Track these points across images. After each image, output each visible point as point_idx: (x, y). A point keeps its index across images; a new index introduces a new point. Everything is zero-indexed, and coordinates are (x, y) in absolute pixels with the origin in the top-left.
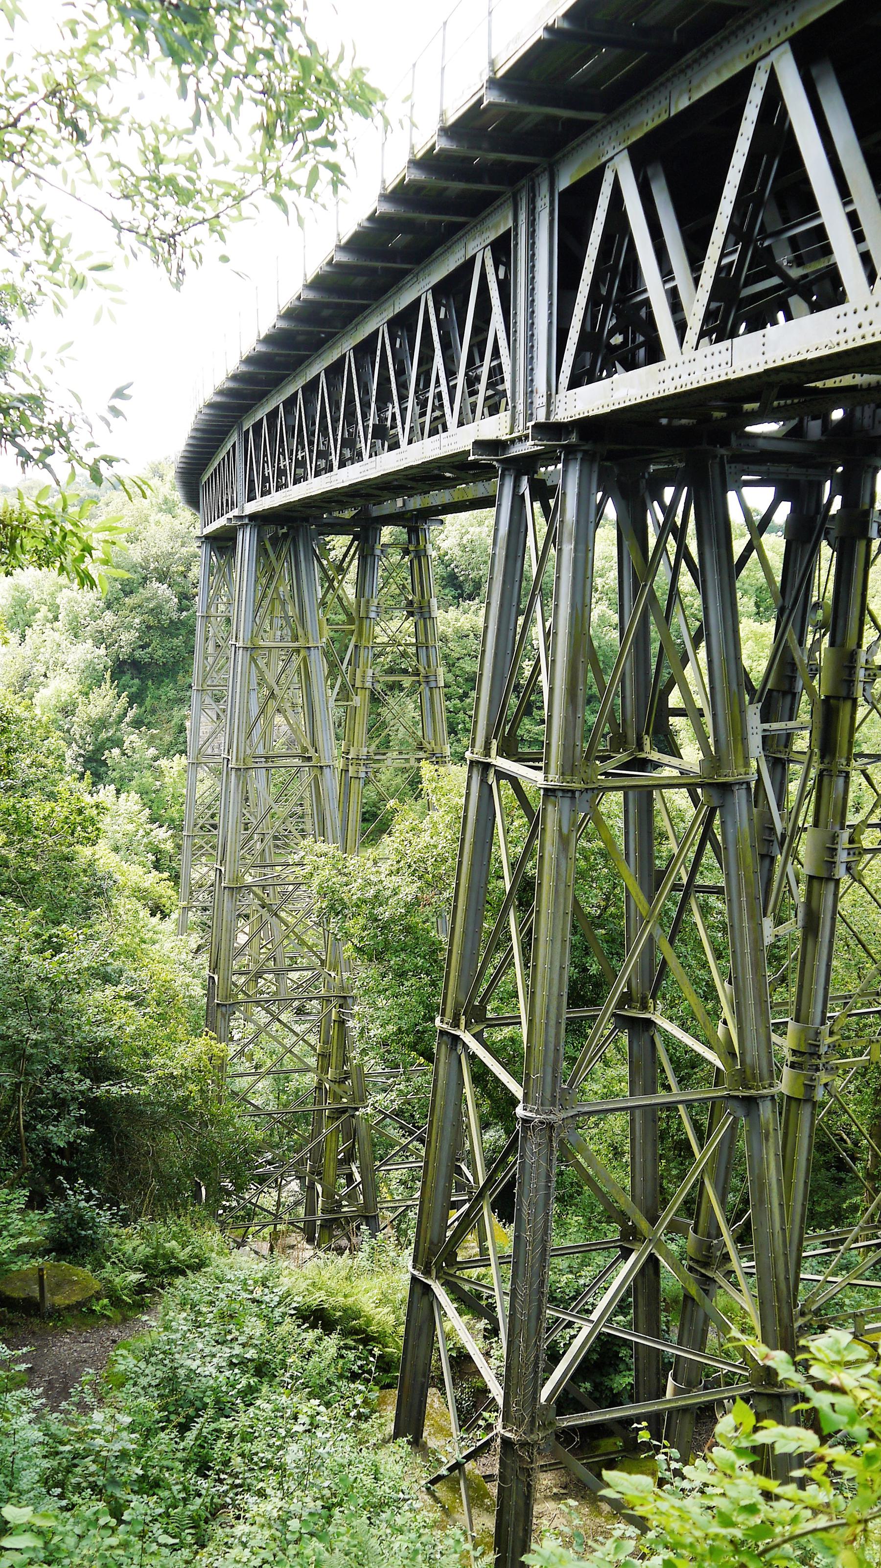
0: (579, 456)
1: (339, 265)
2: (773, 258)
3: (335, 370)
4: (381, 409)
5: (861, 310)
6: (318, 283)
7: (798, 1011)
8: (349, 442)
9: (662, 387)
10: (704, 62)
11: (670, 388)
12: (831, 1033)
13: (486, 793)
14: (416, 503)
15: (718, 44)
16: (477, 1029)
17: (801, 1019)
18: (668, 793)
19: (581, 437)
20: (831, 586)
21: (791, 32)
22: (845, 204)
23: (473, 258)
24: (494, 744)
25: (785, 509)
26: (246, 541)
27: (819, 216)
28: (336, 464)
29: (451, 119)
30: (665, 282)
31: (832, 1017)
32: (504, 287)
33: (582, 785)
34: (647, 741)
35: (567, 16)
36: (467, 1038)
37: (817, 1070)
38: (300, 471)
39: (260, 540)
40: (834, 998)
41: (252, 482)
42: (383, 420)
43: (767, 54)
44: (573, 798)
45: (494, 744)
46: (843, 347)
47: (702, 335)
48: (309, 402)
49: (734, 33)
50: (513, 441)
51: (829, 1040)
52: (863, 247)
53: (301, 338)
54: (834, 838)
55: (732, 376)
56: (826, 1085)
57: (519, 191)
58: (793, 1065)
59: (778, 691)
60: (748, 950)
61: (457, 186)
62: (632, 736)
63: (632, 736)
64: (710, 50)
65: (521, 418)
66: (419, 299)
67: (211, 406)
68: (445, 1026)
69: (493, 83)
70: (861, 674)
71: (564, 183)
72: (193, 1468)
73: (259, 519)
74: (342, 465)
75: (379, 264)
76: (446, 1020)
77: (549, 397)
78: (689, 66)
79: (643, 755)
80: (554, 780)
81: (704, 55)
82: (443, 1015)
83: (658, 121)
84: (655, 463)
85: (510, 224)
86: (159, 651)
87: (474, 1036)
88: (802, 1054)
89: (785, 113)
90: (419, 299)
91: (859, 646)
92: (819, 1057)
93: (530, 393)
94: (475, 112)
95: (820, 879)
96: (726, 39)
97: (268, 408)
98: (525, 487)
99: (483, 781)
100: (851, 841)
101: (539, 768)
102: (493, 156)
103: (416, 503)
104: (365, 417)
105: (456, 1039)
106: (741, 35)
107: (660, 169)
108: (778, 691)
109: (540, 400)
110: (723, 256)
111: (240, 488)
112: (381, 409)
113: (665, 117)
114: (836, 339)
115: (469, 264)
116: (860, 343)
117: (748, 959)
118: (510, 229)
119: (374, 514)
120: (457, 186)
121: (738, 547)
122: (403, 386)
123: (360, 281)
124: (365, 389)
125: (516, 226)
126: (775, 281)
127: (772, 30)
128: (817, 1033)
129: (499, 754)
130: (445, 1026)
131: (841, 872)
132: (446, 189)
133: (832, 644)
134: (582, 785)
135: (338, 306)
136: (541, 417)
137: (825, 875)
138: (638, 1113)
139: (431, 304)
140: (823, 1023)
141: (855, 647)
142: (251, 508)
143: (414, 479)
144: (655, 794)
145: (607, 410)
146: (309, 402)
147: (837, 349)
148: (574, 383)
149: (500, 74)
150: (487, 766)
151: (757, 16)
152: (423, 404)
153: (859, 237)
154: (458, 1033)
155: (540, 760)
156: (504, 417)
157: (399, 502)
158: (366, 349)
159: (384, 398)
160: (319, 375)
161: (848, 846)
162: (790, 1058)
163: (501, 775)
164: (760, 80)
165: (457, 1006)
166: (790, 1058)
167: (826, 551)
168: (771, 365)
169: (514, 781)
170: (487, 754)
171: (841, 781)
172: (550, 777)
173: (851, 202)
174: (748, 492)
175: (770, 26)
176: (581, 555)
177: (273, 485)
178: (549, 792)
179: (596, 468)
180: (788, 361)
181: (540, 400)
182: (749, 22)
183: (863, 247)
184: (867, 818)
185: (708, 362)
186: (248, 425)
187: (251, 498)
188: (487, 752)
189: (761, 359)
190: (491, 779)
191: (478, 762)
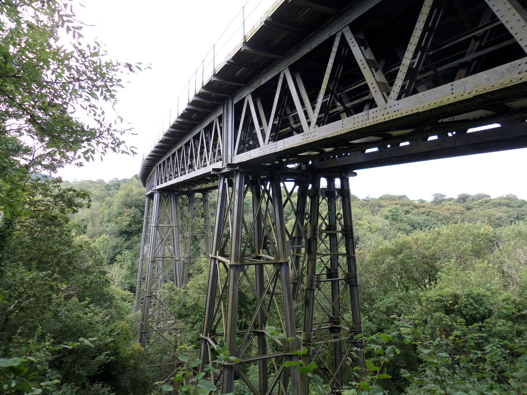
0: (239, 173)
1: (178, 122)
2: (289, 122)
3: (180, 150)
4: (191, 161)
5: (307, 134)
6: (173, 126)
7: (304, 328)
8: (183, 170)
9: (260, 154)
10: (268, 72)
11: (262, 154)
12: (314, 335)
13: (215, 265)
14: (204, 186)
15: (271, 68)
16: (213, 337)
17: (305, 330)
18: (267, 265)
19: (240, 167)
20: (309, 209)
21: (288, 66)
22: (306, 110)
23: (214, 121)
24: (218, 252)
25: (297, 187)
26: (156, 196)
27: (297, 111)
28: (179, 175)
29: (205, 84)
30: (260, 128)
31: (314, 330)
32: (221, 128)
33: (241, 264)
34: (261, 251)
35: (232, 58)
36: (209, 340)
37: (310, 346)
38: (171, 177)
39: (160, 197)
40: (314, 324)
41: (158, 180)
42: (192, 164)
43: (283, 70)
44: (238, 267)
45: (218, 252)
46: (303, 144)
47: (269, 140)
48: (173, 159)
49: (275, 65)
50: (223, 169)
51: (313, 337)
52: (308, 120)
53: (171, 141)
54: (312, 278)
55: (276, 151)
56: (313, 350)
57: (225, 104)
58: (303, 345)
59: (312, 239)
60: (288, 311)
61: (208, 102)
62: (257, 249)
63: (257, 249)
64: (270, 69)
65: (224, 162)
66: (200, 132)
67: (147, 159)
68: (203, 336)
69: (215, 75)
70: (318, 232)
71: (235, 101)
72: (370, 331)
73: (161, 191)
74: (181, 175)
75: (189, 122)
76: (204, 334)
77: (232, 157)
78: (265, 73)
79: (259, 255)
80: (233, 262)
81: (268, 70)
82: (203, 333)
83: (258, 87)
84: (262, 175)
85: (222, 112)
86: (134, 227)
87: (212, 339)
88: (306, 341)
89: (288, 86)
90: (200, 132)
91: (317, 224)
92: (311, 342)
93: (227, 156)
94: (210, 83)
95: (309, 289)
96: (273, 66)
97: (163, 160)
98: (226, 181)
99: (215, 263)
100: (317, 279)
101: (228, 259)
102: (216, 94)
103: (204, 186)
104: (187, 162)
105: (206, 340)
106: (277, 65)
107: (259, 99)
108: (312, 239)
109: (229, 158)
110: (274, 121)
111: (155, 183)
112: (191, 161)
113: (259, 86)
114: (301, 141)
115: (213, 122)
116: (307, 142)
117: (288, 313)
118: (222, 114)
119: (193, 189)
120: (208, 102)
121: (284, 199)
122: (196, 155)
123: (185, 126)
124: (187, 155)
125: (224, 113)
126: (289, 128)
127: (284, 64)
128: (310, 335)
129: (219, 255)
130: (203, 336)
131: (315, 287)
132: (206, 102)
133: (310, 224)
134: (241, 264)
135: (180, 133)
136: (230, 162)
137: (310, 288)
138: (261, 361)
139: (203, 133)
140: (311, 332)
141: (316, 225)
142: (158, 187)
143: (200, 179)
144: (264, 265)
145: (246, 160)
146: (173, 159)
147: (301, 144)
148: (238, 153)
149: (216, 73)
150: (215, 259)
151: (281, 61)
152: (201, 159)
153: (307, 118)
154: (206, 338)
155: (229, 257)
156: (220, 162)
157: (200, 186)
158: (187, 144)
159: (192, 157)
160: (176, 152)
161: (316, 280)
162: (303, 343)
163: (220, 261)
164: (282, 76)
165: (207, 329)
166: (303, 343)
167: (308, 200)
168: (286, 148)
169: (224, 263)
170: (216, 255)
171: (353, 259)
172: (232, 261)
173: (305, 107)
174: (286, 183)
175: (283, 63)
176: (240, 199)
177: (163, 181)
178: (231, 266)
179: (244, 176)
180: (290, 147)
181: (229, 158)
182: (278, 62)
183: (308, 120)
184: (321, 272)
185: (272, 147)
186: (158, 165)
187: (158, 185)
188: (216, 255)
189: (283, 147)
190: (217, 262)
191: (213, 258)
